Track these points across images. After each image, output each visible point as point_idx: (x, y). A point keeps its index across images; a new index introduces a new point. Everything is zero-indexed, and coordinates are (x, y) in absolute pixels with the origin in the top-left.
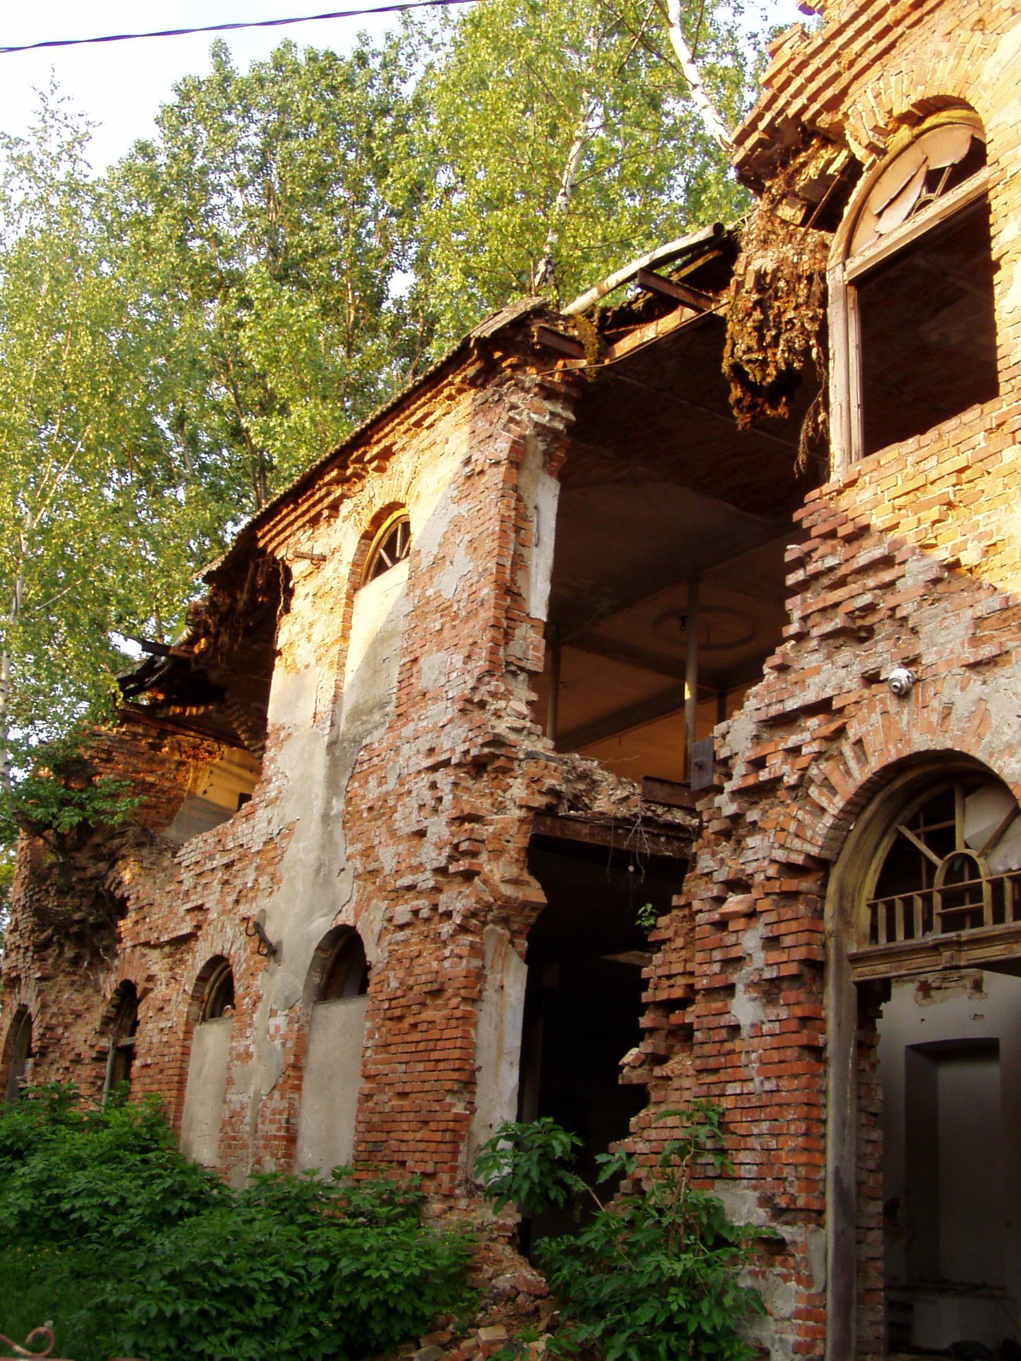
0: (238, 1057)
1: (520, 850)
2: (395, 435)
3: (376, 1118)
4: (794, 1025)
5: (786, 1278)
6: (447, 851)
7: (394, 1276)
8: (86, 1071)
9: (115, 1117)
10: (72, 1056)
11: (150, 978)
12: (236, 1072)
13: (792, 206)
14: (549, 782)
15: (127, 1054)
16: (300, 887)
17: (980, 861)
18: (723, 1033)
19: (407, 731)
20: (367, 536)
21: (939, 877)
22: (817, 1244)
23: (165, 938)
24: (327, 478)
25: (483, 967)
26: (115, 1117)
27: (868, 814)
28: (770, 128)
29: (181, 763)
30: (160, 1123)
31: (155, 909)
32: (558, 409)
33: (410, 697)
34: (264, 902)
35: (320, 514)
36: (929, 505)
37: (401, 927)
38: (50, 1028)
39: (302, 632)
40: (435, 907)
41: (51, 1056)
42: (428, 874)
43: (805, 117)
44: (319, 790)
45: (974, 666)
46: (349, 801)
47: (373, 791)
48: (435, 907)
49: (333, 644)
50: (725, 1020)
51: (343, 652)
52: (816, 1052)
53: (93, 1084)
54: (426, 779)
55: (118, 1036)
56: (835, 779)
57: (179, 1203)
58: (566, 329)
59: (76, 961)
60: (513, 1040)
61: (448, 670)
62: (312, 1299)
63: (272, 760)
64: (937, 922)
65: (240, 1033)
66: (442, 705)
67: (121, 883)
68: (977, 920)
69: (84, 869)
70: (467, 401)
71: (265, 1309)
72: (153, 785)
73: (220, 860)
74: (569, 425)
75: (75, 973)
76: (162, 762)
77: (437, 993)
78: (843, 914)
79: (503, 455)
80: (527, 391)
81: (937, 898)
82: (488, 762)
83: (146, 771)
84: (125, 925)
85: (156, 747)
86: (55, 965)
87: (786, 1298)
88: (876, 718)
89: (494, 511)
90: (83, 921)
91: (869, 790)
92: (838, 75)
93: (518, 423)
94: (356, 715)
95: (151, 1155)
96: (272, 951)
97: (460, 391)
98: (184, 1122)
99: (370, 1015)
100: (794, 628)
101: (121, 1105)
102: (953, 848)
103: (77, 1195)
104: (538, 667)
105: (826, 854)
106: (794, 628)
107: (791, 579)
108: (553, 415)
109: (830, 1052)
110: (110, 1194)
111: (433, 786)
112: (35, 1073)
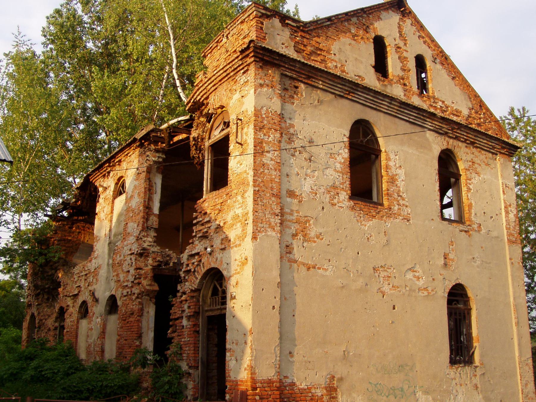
0: (90, 329)
1: (151, 277)
2: (121, 157)
3: (120, 346)
4: (192, 326)
5: (190, 381)
6: (134, 277)
7: (115, 385)
8: (52, 333)
9: (59, 347)
10: (48, 328)
11: (68, 306)
12: (89, 333)
13: (203, 117)
14: (158, 259)
15: (62, 328)
16: (103, 283)
18: (181, 327)
19: (125, 243)
20: (117, 184)
22: (197, 374)
23: (71, 295)
24: (106, 165)
25: (143, 307)
26: (59, 347)
27: (207, 279)
28: (193, 102)
29: (79, 232)
30: (71, 348)
31: (68, 286)
32: (160, 155)
33: (125, 234)
34: (95, 286)
35: (105, 174)
36: (216, 210)
37: (125, 296)
38: (41, 320)
39: (102, 207)
40: (131, 292)
41: (42, 329)
42: (130, 283)
43: (201, 101)
44: (106, 256)
45: (222, 249)
46: (113, 260)
47: (118, 259)
48: (131, 292)
49: (111, 213)
50: (182, 324)
51: (112, 217)
52: (198, 332)
53: (54, 337)
54: (129, 257)
55: (60, 322)
57: (71, 370)
58: (160, 134)
59: (48, 299)
60: (152, 325)
61: (134, 228)
62: (98, 392)
63: (96, 246)
64: (220, 304)
65: (90, 323)
66: (133, 237)
67: (59, 277)
69: (48, 272)
70: (138, 150)
71: (86, 394)
72: (70, 240)
73: (84, 273)
74: (163, 159)
75: (48, 303)
76: (73, 233)
77: (133, 314)
79: (145, 170)
80: (152, 151)
81: (220, 298)
82: (143, 254)
83: (68, 236)
84: (60, 290)
85: (71, 228)
86: (42, 301)
87: (191, 385)
88: (206, 258)
89: (143, 186)
90: (49, 288)
92: (206, 93)
93: (149, 161)
94: (115, 235)
95: (68, 358)
96: (97, 300)
97: (136, 148)
98: (78, 348)
99: (119, 319)
100: (194, 234)
101: (60, 343)
103: (46, 370)
104: (157, 227)
105: (199, 288)
106: (194, 234)
107: (195, 222)
108: (159, 157)
109: (200, 332)
110: (55, 369)
111: (131, 259)
112: (37, 334)
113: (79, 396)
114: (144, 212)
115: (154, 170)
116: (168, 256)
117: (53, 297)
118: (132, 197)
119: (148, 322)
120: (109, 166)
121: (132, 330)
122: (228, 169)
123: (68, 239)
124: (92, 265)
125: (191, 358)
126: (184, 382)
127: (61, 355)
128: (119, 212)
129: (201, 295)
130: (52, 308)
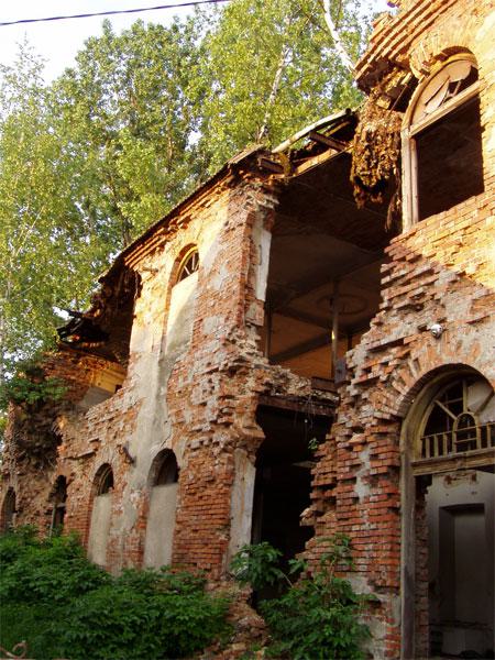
2: (192, 211)
5: (381, 620)
6: (217, 413)
8: (42, 520)
10: (35, 512)
11: (73, 474)
14: (267, 379)
15: (62, 511)
16: (145, 429)
17: (475, 418)
19: (197, 355)
20: (178, 260)
21: (455, 426)
22: (396, 603)
28: (373, 62)
30: (77, 545)
32: (271, 198)
34: (128, 438)
36: (450, 245)
37: (195, 450)
39: (146, 307)
41: (25, 512)
42: (208, 424)
43: (390, 57)
44: (155, 383)
47: (181, 384)
48: (211, 440)
52: (396, 510)
54: (207, 378)
56: (405, 378)
59: (37, 466)
60: (249, 505)
62: (151, 630)
64: (454, 447)
65: (116, 501)
68: (474, 446)
69: (41, 421)
70: (226, 194)
71: (129, 635)
72: (74, 380)
77: (212, 481)
78: (409, 443)
79: (244, 221)
81: (454, 436)
82: (236, 370)
85: (76, 362)
86: (27, 469)
88: (425, 348)
91: (421, 383)
92: (406, 36)
93: (251, 205)
94: (173, 346)
95: (73, 560)
97: (223, 190)
98: (89, 545)
100: (385, 305)
102: (462, 411)
103: (37, 580)
105: (400, 414)
106: (385, 305)
107: (383, 281)
108: (268, 201)
109: (402, 510)
111: (210, 381)
112: (17, 521)
113: (115, 639)
114: (241, 294)
115: (259, 224)
116: (283, 377)
117: (46, 462)
118: (212, 273)
119: (242, 497)
120: (164, 233)
121: (210, 512)
122: (481, 158)
123: (69, 379)
124: (122, 403)
125: (382, 568)
126: (361, 622)
127: (61, 556)
128: (182, 305)
129: (403, 430)
130: (43, 481)
